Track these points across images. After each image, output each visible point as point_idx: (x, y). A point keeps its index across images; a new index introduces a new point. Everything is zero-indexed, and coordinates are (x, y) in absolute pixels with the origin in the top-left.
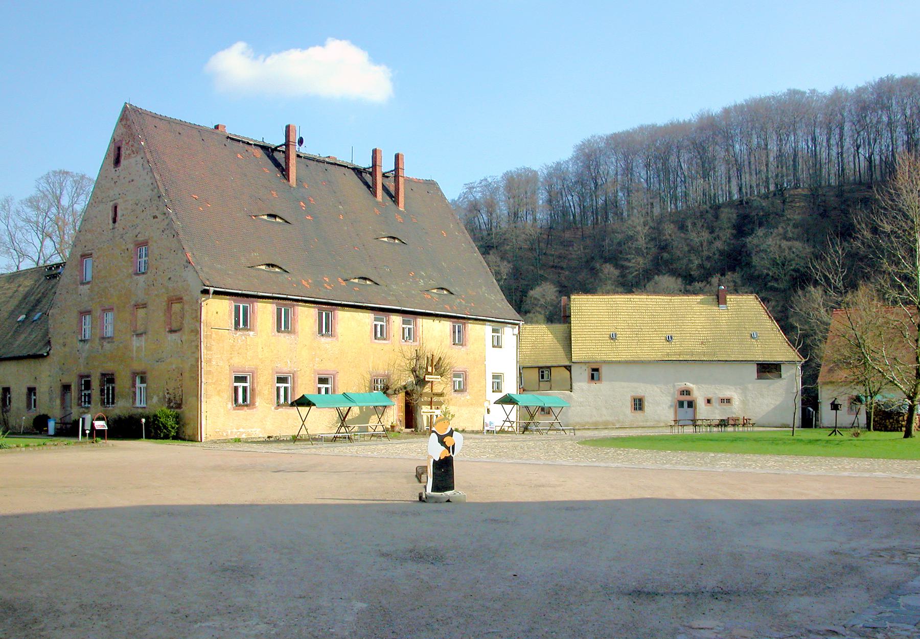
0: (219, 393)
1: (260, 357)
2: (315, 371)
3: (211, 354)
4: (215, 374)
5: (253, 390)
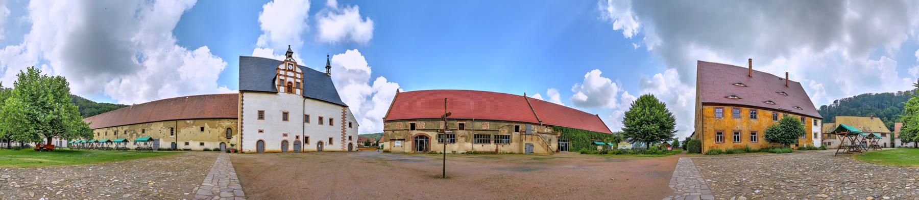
0: (710, 138)
1: (726, 125)
5: (724, 137)
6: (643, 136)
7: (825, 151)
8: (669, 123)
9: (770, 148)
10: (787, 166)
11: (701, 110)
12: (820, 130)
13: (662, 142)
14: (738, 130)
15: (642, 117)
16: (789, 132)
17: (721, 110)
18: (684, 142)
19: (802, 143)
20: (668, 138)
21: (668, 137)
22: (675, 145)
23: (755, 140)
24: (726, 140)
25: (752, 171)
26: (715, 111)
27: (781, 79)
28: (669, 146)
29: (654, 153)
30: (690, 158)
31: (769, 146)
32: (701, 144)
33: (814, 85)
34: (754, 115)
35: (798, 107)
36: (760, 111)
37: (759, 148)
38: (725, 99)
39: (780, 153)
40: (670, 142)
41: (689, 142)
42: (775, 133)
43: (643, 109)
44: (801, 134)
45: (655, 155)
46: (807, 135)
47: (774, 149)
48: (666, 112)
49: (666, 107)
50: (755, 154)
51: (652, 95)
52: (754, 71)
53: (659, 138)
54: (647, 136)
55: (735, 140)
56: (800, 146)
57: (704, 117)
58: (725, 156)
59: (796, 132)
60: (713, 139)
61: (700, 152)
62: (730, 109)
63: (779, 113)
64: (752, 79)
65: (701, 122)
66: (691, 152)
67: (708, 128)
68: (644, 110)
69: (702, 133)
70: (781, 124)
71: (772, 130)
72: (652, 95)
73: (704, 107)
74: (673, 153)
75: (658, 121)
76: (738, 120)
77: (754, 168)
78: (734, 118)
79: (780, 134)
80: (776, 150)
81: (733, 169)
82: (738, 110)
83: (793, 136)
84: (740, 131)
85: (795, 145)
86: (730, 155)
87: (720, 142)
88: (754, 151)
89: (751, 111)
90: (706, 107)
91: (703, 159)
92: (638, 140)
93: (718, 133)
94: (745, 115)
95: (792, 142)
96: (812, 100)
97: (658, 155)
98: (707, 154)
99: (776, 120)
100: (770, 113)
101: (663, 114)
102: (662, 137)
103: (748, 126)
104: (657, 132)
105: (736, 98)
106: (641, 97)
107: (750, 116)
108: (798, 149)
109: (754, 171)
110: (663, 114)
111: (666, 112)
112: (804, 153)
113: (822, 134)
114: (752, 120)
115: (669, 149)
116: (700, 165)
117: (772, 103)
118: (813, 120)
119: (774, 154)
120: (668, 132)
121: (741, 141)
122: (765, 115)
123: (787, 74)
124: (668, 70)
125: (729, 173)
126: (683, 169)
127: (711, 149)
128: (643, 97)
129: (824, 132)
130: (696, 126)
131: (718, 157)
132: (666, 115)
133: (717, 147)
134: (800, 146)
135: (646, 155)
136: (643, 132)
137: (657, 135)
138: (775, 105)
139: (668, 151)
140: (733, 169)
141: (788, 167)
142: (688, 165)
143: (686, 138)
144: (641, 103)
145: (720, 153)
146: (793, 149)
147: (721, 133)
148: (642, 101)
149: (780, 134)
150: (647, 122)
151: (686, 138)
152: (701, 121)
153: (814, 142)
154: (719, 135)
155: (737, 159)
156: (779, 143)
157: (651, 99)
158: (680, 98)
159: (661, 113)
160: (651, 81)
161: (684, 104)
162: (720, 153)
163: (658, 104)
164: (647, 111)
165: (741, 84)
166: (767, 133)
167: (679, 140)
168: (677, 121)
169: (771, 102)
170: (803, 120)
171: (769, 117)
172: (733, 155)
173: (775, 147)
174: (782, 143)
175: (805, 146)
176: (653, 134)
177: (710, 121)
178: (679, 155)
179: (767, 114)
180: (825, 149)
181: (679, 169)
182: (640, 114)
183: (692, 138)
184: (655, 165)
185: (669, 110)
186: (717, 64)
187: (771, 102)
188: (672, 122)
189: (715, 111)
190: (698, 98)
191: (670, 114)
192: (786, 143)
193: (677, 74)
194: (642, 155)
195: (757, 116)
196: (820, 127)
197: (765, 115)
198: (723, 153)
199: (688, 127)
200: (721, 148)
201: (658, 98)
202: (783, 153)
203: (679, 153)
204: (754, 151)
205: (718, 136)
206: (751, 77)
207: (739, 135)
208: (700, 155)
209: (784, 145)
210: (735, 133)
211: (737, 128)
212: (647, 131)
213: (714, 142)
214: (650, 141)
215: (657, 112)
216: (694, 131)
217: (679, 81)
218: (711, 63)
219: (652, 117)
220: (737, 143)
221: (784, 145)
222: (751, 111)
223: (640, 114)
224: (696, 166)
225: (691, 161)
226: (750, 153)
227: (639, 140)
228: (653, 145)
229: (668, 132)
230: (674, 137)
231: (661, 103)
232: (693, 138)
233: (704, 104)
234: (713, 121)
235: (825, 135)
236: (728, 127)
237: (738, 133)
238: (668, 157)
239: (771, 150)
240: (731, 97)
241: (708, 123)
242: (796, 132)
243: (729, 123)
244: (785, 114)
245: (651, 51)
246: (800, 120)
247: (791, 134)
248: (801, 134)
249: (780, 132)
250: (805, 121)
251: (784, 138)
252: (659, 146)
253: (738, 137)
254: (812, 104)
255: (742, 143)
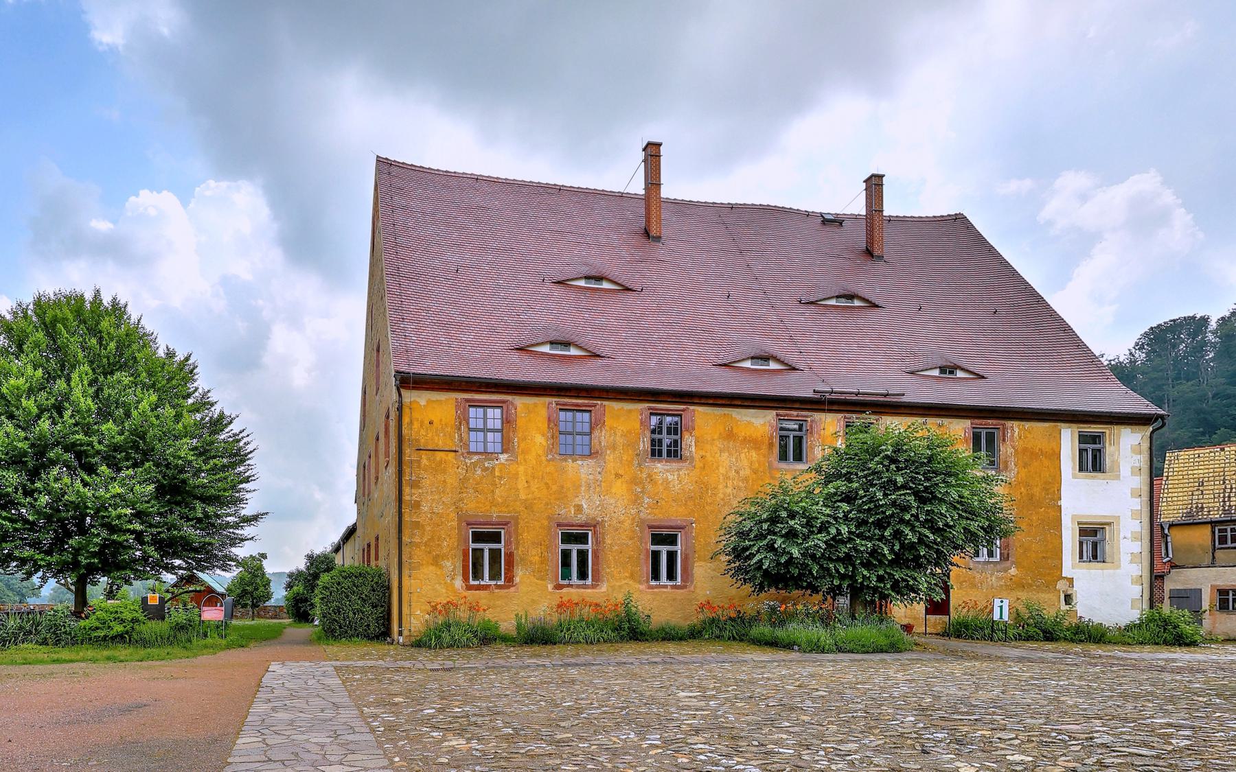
0: (436, 561)
1: (522, 496)
2: (642, 522)
3: (420, 495)
4: (428, 528)
5: (510, 556)
6: (47, 538)
7: (1181, 656)
8: (214, 470)
9: (756, 619)
10: (869, 730)
11: (393, 415)
12: (1139, 504)
13: (169, 578)
14: (582, 518)
15: (45, 425)
16: (880, 525)
17: (494, 414)
18: (295, 577)
19: (977, 597)
20: (207, 557)
21: (203, 548)
22: (244, 592)
23: (671, 576)
24: (520, 574)
25: (654, 738)
26: (463, 419)
27: (832, 222)
28: (209, 596)
29: (120, 638)
30: (328, 666)
31: (750, 607)
32: (389, 588)
33: (1084, 198)
34: (667, 440)
35: (948, 369)
36: (701, 415)
37: (695, 620)
38: (515, 356)
39: (817, 648)
40: (219, 579)
41: (325, 578)
42: (791, 535)
43: (50, 377)
44: (971, 537)
45: (122, 651)
46: (1018, 539)
47: (782, 623)
48: (195, 409)
49: (202, 382)
50: (671, 647)
51: (115, 303)
52: (675, 202)
53: (151, 550)
54: (74, 541)
55: (566, 575)
56: (957, 610)
57: (407, 451)
58: (512, 657)
59: (931, 524)
60: (452, 565)
61: (384, 634)
62: (544, 413)
63: (818, 416)
64: (660, 251)
65: (389, 475)
66: (335, 631)
67: (425, 508)
68: (61, 384)
69: (394, 531)
70: (829, 479)
71: (774, 520)
72: (115, 303)
73: (409, 396)
74: (233, 637)
75: (147, 454)
76: (582, 470)
77: (663, 723)
78: (564, 456)
79: (819, 540)
80: (794, 630)
81: (554, 724)
82: (587, 415)
83: (912, 546)
84: (594, 525)
85: (920, 608)
86: (537, 649)
87: (486, 580)
88: (668, 636)
89: (654, 420)
90: (418, 399)
91: (397, 670)
92: (10, 557)
93: (478, 537)
94: (620, 440)
95: (904, 590)
96: (1059, 302)
97: (142, 652)
98: (419, 644)
99: (799, 457)
100: (761, 422)
101: (178, 417)
102: (171, 546)
103: (636, 500)
104: (139, 515)
105: (573, 352)
106: (38, 303)
107: (645, 444)
108: (945, 634)
109: (666, 743)
110: (178, 417)
111: (195, 409)
112: (989, 658)
113: (1158, 533)
114: (660, 467)
115: (212, 614)
116: (379, 703)
117: (773, 366)
118: (1068, 439)
119: (782, 655)
120: (205, 523)
121: (597, 578)
122: (730, 435)
123: (874, 185)
124: (212, 183)
125: (532, 747)
126: (291, 723)
127: (440, 620)
128: (57, 304)
129: (1170, 512)
130: (363, 496)
131: (477, 660)
132: (200, 425)
133: (473, 608)
134: (957, 610)
135: (65, 654)
136: (51, 516)
137: (139, 536)
138: (794, 375)
139: (204, 630)
140: (554, 724)
141: (873, 740)
142: (316, 702)
143: (310, 557)
144: (40, 335)
145: (487, 638)
146: (908, 628)
147: (495, 538)
148: (50, 328)
149: (819, 540)
150: (79, 455)
151: (310, 557)
152: (392, 469)
153: (1079, 591)
154: (486, 547)
155: (574, 672)
156: (815, 590)
157: (104, 324)
158: (281, 340)
159: (169, 412)
160: (115, 222)
161: (299, 378)
162: (487, 638)
163: (151, 357)
164: (77, 393)
165: (599, 279)
166: (743, 535)
167: (269, 568)
168: (258, 464)
169: (766, 359)
170: (985, 443)
171: (754, 443)
172: (557, 649)
173: (792, 616)
174: (835, 592)
175: (1002, 611)
176: (112, 529)
177: (439, 468)
178: (266, 650)
179: (742, 432)
180: (1181, 641)
181: (264, 725)
182: (29, 404)
183: (338, 560)
184: (129, 710)
185: (213, 397)
186: (477, 179)
187: (766, 359)
188: (233, 465)
189: (463, 419)
190: (374, 349)
191: (219, 423)
192: (856, 592)
193: (264, 212)
194: (42, 652)
195: (688, 441)
196: (1140, 482)
197: (730, 435)
198: (505, 639)
199: (318, 496)
200: (489, 615)
201: (148, 325)
202: (840, 650)
203: (270, 636)
204: (668, 636)
205: (478, 553)
206: (658, 239)
207: (589, 547)
208: (375, 648)
209: (844, 601)
210: (568, 538)
211: (579, 508)
212: (79, 508)
213: (459, 583)
214: (92, 570)
215: (144, 405)
216: (351, 517)
217: (276, 255)
218: (447, 175)
219: (109, 427)
220: (575, 592)
221: (844, 601)
222: (654, 420)
223: (29, 404)
224: (359, 708)
225: (335, 682)
226: (641, 646)
227: (23, 561)
228: (110, 594)
229: (205, 523)
230: (241, 552)
231: (170, 354)
232: (348, 559)
233: (407, 381)
234: (454, 470)
235: (1176, 536)
236: (529, 506)
237: (582, 539)
238: (205, 659)
239: (763, 630)
240: (546, 349)
241: (426, 483)
242: (931, 524)
243: (535, 486)
244: (857, 419)
245: (112, 50)
246: (964, 450)
247: (897, 534)
248: (971, 537)
249: (823, 528)
250: (1006, 450)
251: (847, 560)
252: (153, 600)
253: (582, 555)
254: (1066, 329)
255: (604, 588)
